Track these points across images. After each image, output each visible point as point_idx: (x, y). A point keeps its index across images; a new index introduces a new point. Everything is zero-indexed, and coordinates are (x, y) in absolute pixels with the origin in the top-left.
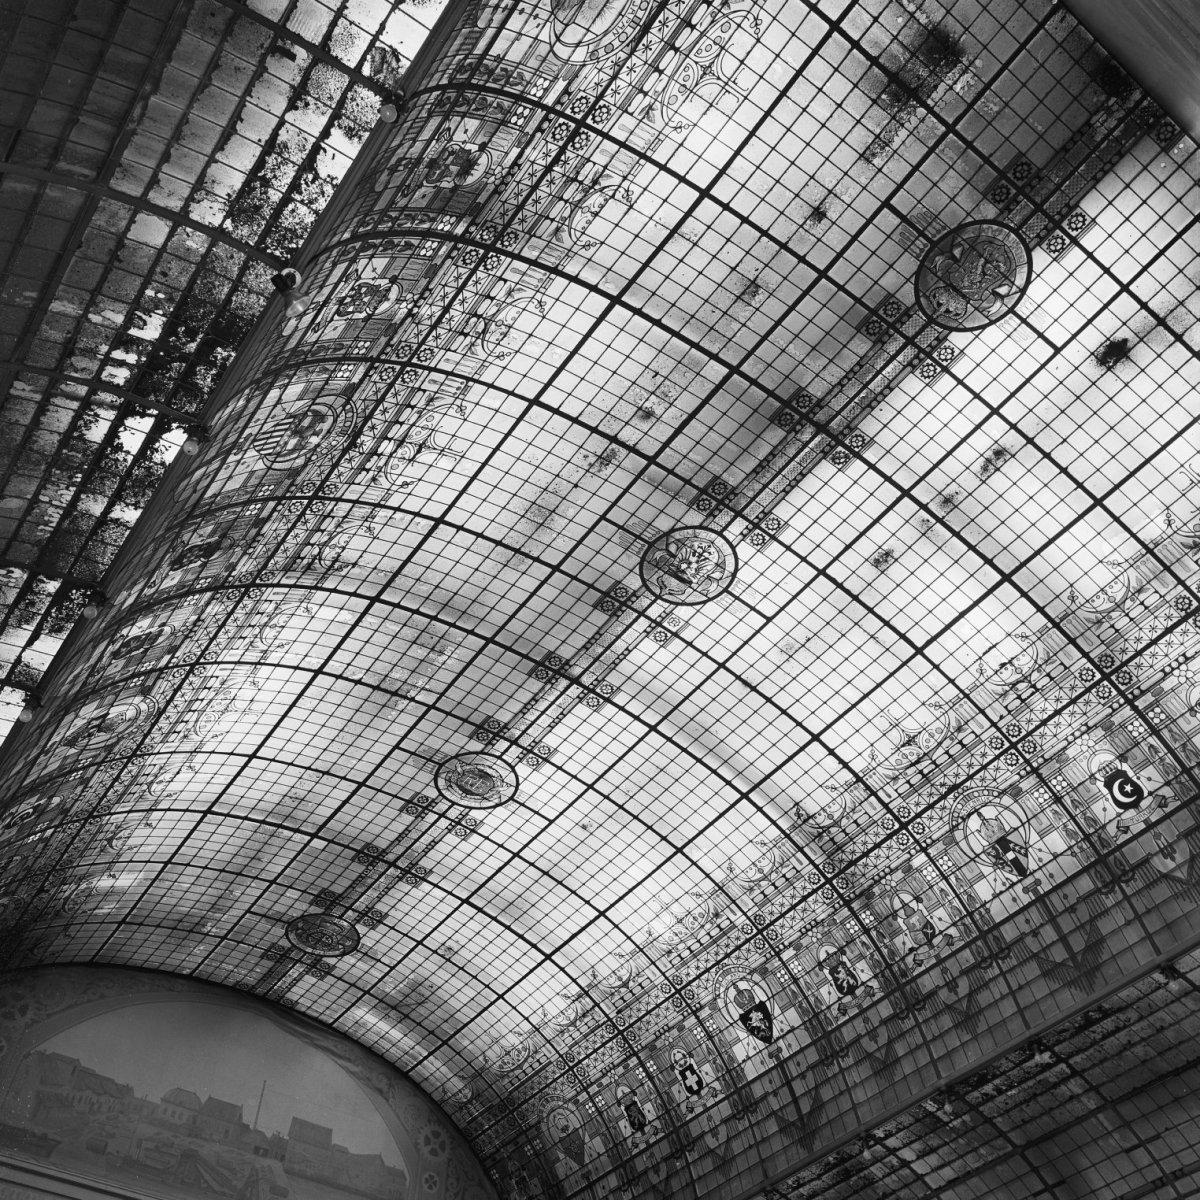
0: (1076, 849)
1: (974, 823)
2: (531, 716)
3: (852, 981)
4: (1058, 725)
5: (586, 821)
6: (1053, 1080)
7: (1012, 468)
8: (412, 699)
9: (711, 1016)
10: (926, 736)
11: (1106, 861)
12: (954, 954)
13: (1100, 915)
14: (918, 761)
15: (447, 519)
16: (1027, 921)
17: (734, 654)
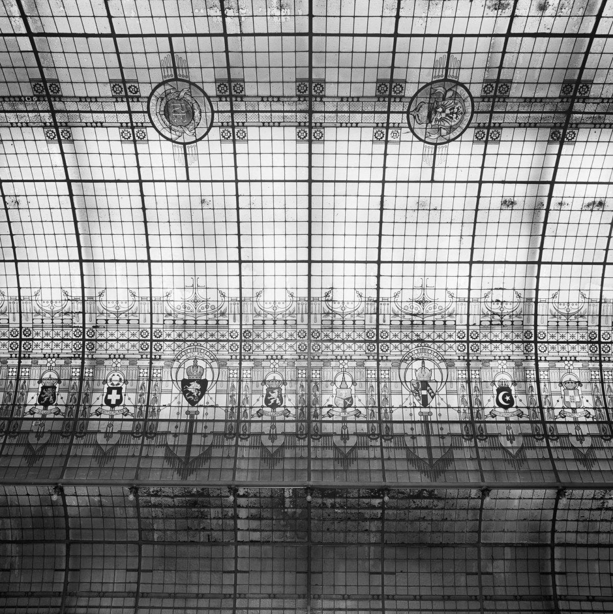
0: (462, 410)
1: (417, 365)
2: (263, 106)
3: (278, 401)
4: (496, 347)
5: (208, 199)
6: (367, 516)
7: (596, 216)
8: (224, 16)
9: (162, 368)
11: (474, 426)
12: (284, 421)
13: (457, 447)
14: (415, 315)
16: (412, 429)
17: (154, 181)
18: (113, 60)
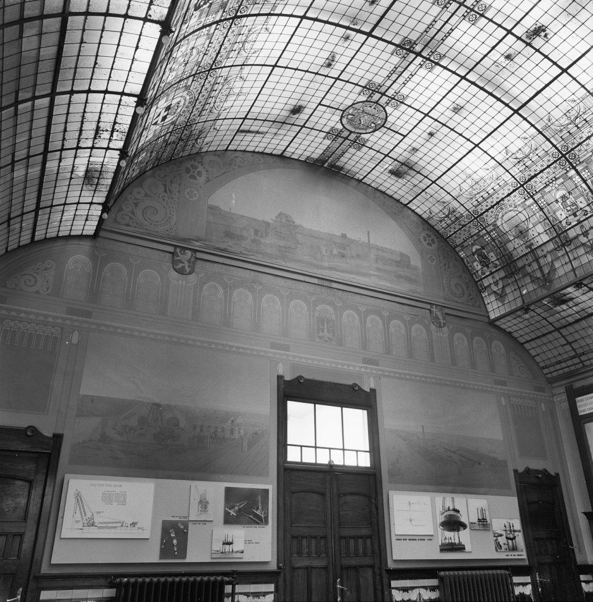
16: (527, 260)
18: (349, 87)
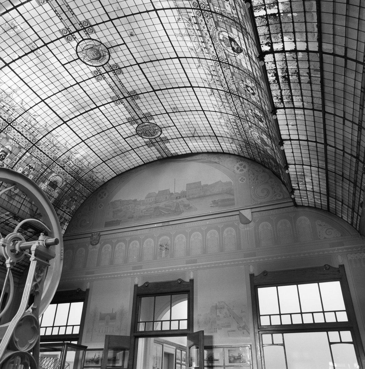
10: (10, 100)
15: (158, 11)
